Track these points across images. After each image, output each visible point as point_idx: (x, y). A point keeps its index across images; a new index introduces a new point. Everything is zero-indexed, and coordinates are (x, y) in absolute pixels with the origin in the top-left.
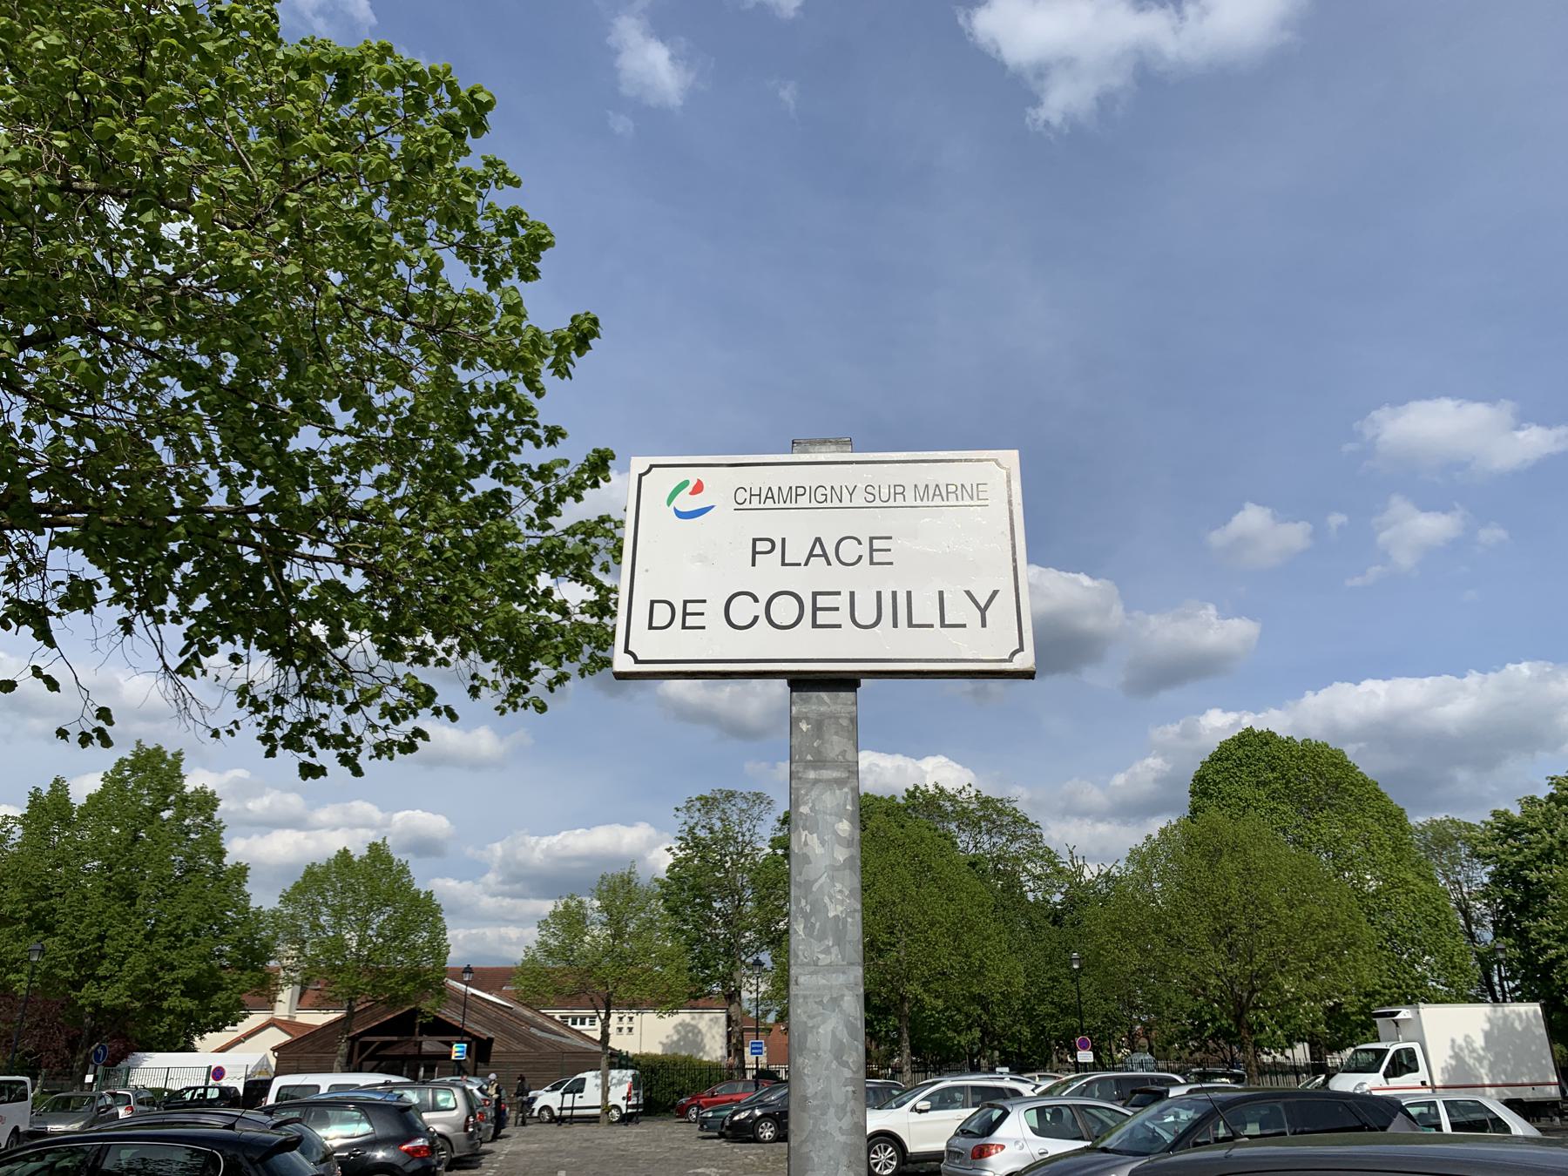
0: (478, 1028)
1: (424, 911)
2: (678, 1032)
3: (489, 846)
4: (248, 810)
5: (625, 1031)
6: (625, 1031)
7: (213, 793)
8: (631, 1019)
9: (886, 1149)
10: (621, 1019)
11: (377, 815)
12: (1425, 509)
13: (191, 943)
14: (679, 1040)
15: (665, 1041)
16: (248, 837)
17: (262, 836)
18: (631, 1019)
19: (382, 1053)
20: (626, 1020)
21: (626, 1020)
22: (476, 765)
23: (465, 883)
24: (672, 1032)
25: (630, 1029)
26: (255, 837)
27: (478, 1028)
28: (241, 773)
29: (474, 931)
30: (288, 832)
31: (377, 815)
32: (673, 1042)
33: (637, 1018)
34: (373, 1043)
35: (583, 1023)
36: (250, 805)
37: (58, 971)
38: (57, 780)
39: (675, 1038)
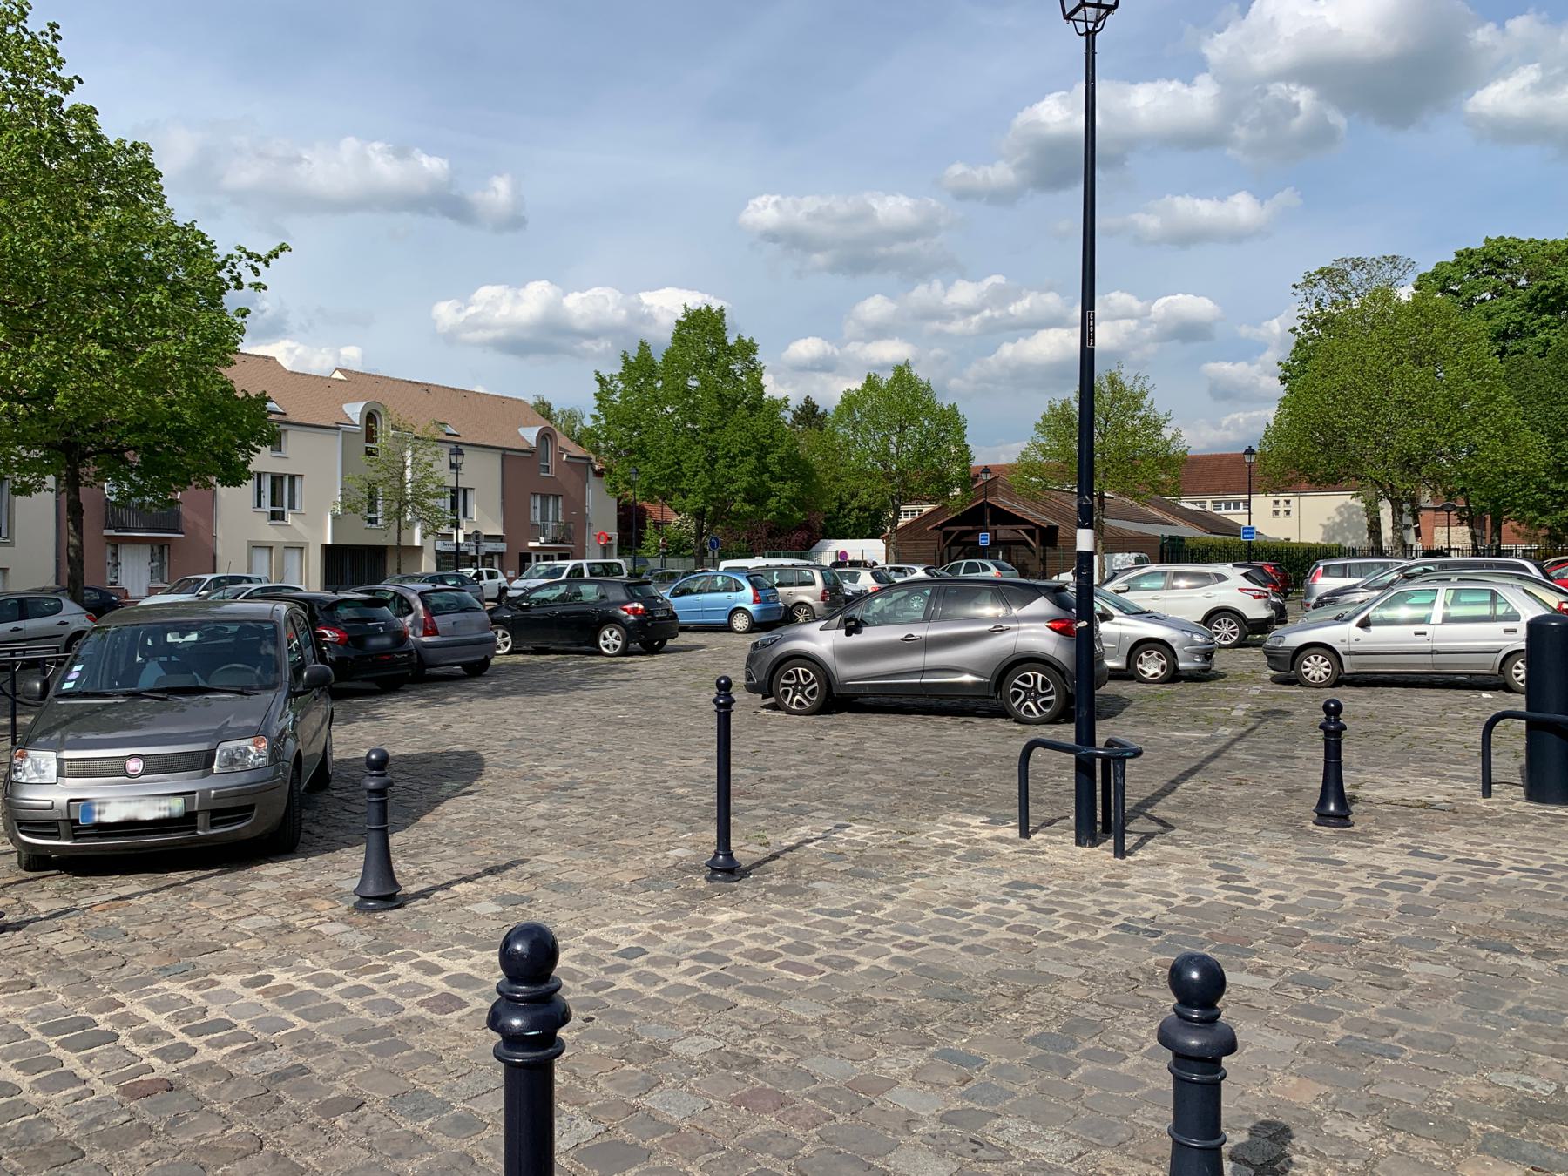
0: (1044, 517)
1: (951, 422)
2: (1340, 514)
3: (1265, 324)
4: (1011, 316)
5: (1282, 513)
6: (1282, 513)
7: (752, 340)
8: (1288, 502)
9: (1230, 623)
10: (1277, 502)
11: (1137, 305)
12: (430, 154)
13: (741, 462)
14: (1341, 521)
15: (1326, 522)
16: (1014, 341)
17: (1027, 338)
18: (1288, 502)
19: (966, 539)
20: (1282, 503)
21: (1282, 503)
22: (1236, 236)
23: (1238, 365)
24: (1334, 514)
25: (1288, 512)
26: (1021, 341)
27: (1044, 517)
28: (998, 279)
29: (1255, 414)
30: (1052, 331)
31: (1137, 305)
32: (1335, 524)
33: (1294, 500)
34: (954, 532)
35: (1227, 507)
36: (1012, 309)
37: (656, 486)
38: (642, 343)
39: (1338, 519)
